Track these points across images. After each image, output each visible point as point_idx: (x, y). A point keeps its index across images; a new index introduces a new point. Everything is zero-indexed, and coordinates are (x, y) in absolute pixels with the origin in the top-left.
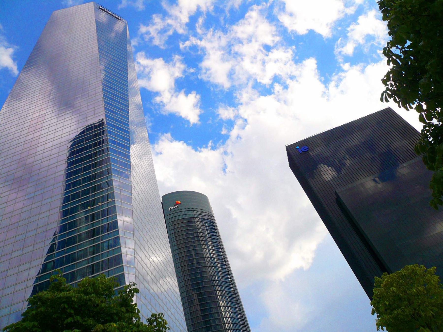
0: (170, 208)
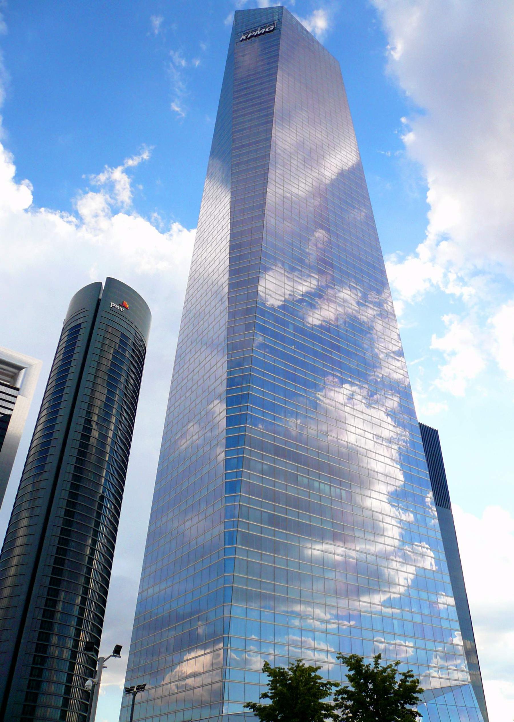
0: (112, 303)
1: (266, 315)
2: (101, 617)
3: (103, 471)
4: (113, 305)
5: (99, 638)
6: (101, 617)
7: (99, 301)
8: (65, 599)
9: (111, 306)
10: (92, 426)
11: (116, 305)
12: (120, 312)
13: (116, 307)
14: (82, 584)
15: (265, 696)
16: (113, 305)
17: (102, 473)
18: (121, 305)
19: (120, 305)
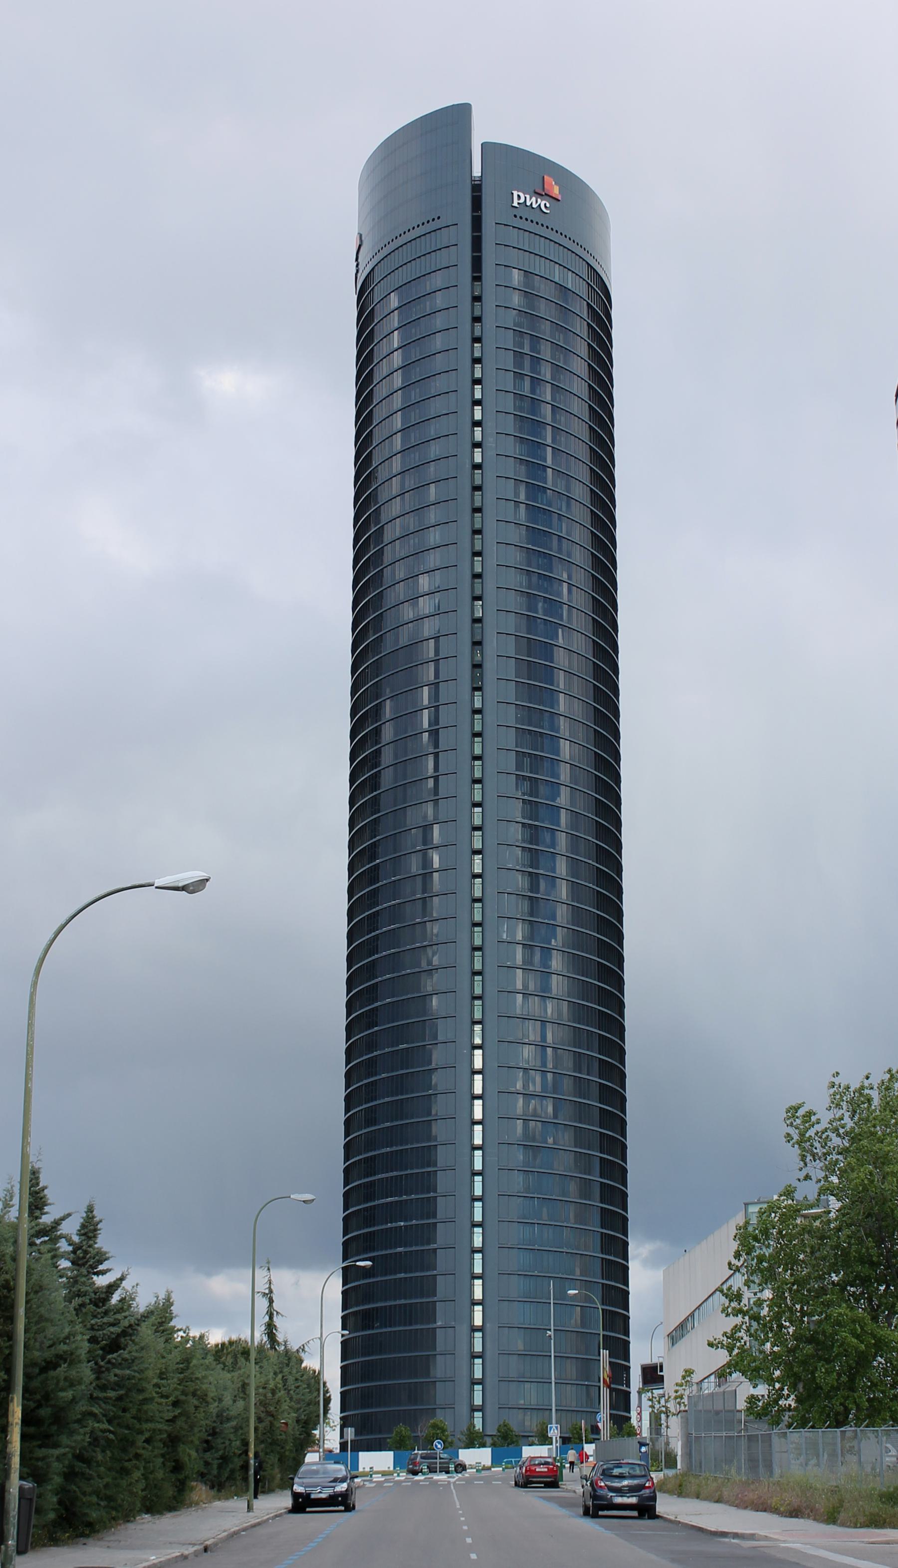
0: (515, 193)
1: (595, 1091)
2: (621, 1211)
3: (545, 451)
4: (519, 197)
5: (625, 1189)
6: (621, 1211)
7: (477, 188)
8: (526, 986)
9: (515, 204)
10: (558, 731)
11: (528, 197)
12: (537, 217)
13: (528, 203)
14: (518, 820)
15: (364, 1468)
16: (519, 197)
17: (560, 594)
18: (540, 191)
19: (538, 194)
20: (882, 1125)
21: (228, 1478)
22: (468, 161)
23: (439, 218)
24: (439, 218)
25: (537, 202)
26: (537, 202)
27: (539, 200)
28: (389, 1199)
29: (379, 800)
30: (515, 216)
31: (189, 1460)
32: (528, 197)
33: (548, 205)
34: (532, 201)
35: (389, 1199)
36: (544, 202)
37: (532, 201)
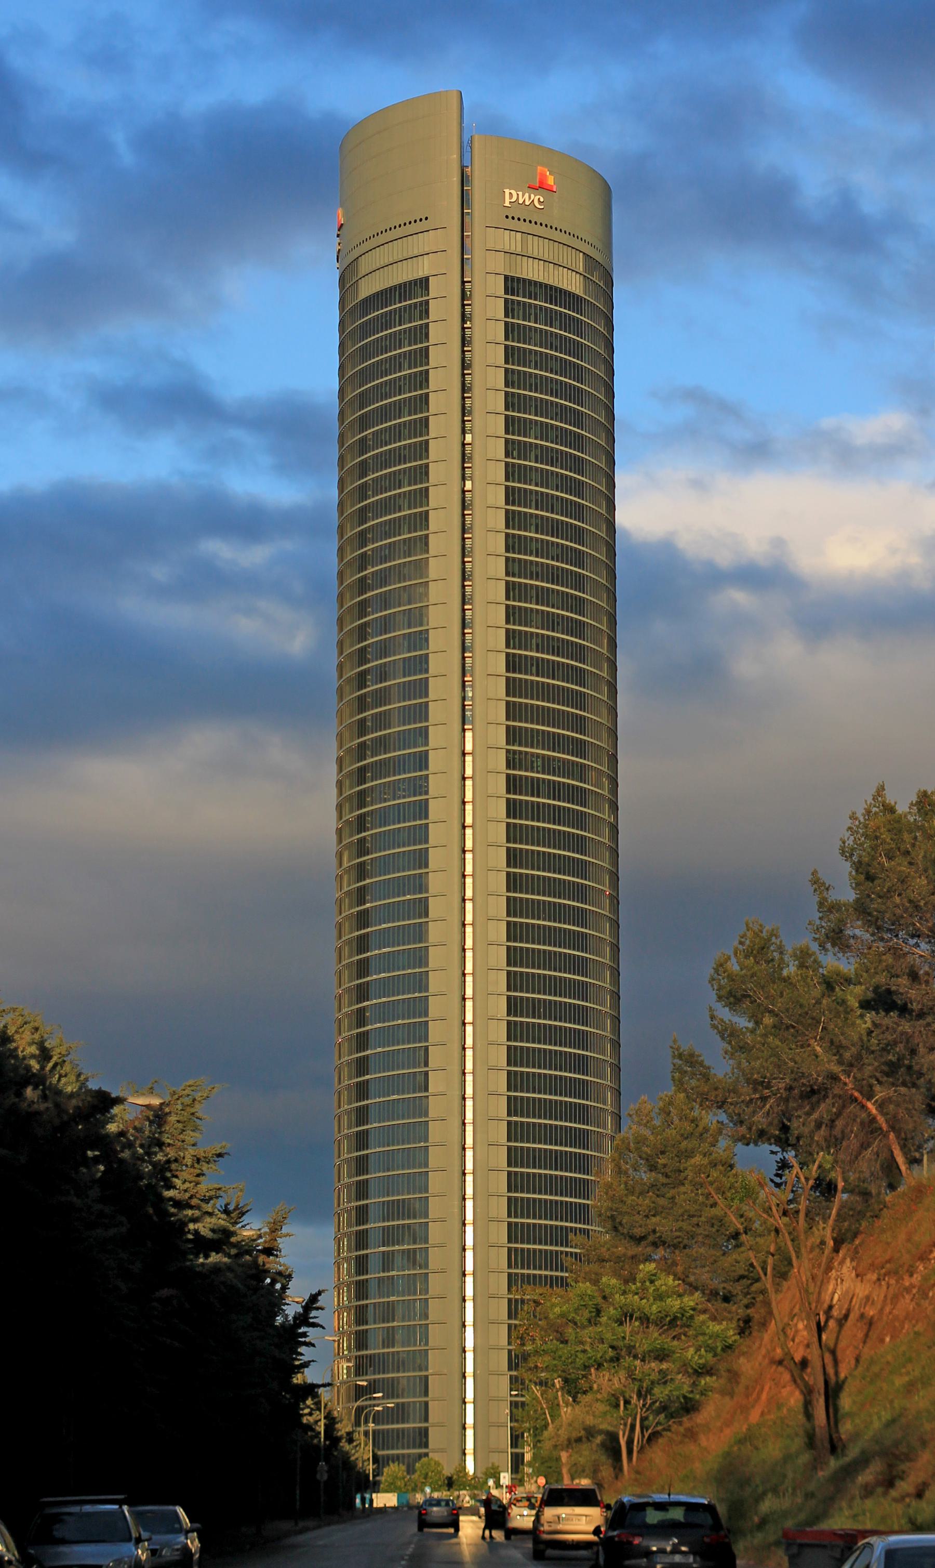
0: (507, 191)
9: (507, 204)
13: (521, 202)
20: (276, 1297)
21: (200, 1210)
22: (478, 1136)
23: (426, 219)
24: (426, 219)
25: (530, 198)
26: (530, 198)
27: (532, 196)
28: (384, 926)
29: (427, 931)
30: (507, 217)
31: (794, 1307)
32: (520, 193)
33: (542, 200)
34: (526, 198)
35: (384, 926)
36: (538, 197)
37: (526, 198)
